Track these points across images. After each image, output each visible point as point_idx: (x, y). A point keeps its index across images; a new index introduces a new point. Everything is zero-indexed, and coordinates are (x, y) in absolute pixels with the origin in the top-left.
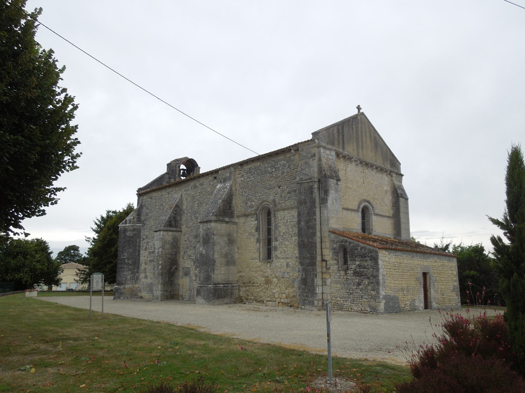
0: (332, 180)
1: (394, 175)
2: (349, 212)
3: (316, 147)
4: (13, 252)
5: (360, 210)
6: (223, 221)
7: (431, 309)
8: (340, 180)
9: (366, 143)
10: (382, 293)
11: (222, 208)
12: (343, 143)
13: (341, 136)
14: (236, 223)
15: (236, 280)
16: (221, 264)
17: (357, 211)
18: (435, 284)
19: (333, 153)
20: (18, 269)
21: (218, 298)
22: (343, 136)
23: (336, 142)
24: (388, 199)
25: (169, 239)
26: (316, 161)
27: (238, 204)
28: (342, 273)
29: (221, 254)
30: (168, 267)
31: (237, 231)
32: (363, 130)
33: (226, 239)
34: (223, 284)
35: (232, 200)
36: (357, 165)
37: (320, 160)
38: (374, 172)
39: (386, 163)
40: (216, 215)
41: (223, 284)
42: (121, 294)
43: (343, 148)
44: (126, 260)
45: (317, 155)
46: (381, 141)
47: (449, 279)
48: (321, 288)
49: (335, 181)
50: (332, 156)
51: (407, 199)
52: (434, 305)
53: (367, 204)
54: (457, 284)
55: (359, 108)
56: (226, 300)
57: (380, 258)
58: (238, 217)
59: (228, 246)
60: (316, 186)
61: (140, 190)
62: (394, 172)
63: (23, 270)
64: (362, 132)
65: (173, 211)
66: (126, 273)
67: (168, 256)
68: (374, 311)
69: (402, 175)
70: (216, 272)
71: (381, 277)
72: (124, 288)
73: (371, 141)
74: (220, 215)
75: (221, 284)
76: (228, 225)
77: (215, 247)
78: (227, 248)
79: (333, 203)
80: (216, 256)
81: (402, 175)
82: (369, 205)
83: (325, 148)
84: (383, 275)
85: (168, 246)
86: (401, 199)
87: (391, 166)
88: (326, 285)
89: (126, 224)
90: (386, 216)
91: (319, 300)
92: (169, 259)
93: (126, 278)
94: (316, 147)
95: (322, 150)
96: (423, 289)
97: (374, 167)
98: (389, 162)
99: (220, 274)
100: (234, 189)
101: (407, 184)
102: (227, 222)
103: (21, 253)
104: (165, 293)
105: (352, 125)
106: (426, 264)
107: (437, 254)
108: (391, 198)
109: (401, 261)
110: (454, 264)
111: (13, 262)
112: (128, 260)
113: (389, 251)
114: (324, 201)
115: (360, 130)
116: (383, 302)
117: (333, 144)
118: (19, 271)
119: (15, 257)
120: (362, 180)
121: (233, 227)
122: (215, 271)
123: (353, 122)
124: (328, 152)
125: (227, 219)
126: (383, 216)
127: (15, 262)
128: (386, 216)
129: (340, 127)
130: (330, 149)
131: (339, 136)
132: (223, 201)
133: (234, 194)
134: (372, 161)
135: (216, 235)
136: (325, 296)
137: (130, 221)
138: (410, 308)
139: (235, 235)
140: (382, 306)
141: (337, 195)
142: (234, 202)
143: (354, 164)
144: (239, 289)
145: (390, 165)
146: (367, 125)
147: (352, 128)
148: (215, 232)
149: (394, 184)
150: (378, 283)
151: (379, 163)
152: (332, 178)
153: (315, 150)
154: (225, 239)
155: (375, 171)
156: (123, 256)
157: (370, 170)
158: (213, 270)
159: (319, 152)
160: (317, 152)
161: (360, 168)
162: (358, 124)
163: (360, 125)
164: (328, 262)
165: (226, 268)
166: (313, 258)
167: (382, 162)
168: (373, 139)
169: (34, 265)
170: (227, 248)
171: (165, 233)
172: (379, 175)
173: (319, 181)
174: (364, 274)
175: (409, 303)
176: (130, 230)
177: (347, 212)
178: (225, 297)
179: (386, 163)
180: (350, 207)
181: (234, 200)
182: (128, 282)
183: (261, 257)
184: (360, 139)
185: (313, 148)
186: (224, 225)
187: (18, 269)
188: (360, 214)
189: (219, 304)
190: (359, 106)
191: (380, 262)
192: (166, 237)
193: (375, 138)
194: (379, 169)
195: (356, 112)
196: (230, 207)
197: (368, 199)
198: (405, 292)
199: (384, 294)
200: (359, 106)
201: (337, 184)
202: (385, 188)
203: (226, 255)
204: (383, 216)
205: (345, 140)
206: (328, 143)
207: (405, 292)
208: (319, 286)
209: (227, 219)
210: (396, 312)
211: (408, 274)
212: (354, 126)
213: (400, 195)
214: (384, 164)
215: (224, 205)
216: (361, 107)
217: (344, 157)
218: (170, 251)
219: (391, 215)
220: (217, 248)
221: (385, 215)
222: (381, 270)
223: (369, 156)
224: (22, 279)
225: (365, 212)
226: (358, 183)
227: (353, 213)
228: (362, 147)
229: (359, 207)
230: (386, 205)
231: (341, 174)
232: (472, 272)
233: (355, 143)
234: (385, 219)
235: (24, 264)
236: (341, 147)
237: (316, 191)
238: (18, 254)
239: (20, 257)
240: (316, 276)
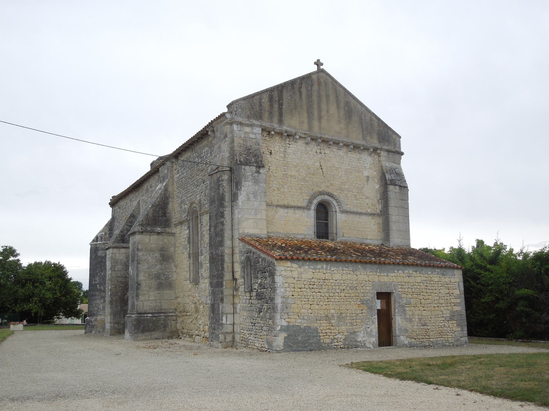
0: (247, 168)
1: (383, 153)
2: (291, 211)
3: (227, 123)
4: (22, 280)
5: (313, 207)
6: (152, 232)
7: (396, 346)
8: (263, 167)
9: (328, 112)
10: (281, 322)
11: (150, 215)
12: (281, 115)
13: (276, 106)
14: (173, 234)
15: (173, 307)
16: (150, 288)
17: (308, 208)
18: (407, 309)
19: (258, 130)
20: (27, 299)
21: (143, 331)
22: (281, 105)
23: (266, 115)
24: (373, 189)
25: (121, 258)
26: (227, 143)
27: (176, 210)
28: (248, 294)
29: (149, 275)
30: (119, 294)
31: (175, 244)
32: (323, 94)
33: (157, 255)
34: (152, 313)
35: (167, 204)
36: (307, 144)
37: (233, 142)
38: (342, 152)
39: (368, 138)
40: (142, 225)
41: (152, 313)
42: (93, 327)
43: (281, 122)
44: (98, 286)
45: (229, 136)
46: (359, 106)
47: (441, 301)
48: (230, 317)
49: (254, 169)
50: (256, 134)
51: (404, 188)
52: (403, 339)
53: (326, 197)
54: (460, 308)
55: (318, 63)
56: (156, 334)
57: (278, 273)
58: (176, 225)
59: (161, 264)
60: (226, 177)
61: (110, 204)
62: (381, 149)
63: (32, 300)
64: (319, 96)
65: (127, 222)
66: (98, 301)
67: (120, 279)
68: (268, 350)
69: (402, 154)
70: (141, 298)
71: (278, 301)
72: (96, 320)
73: (338, 107)
74: (149, 225)
75: (149, 313)
76: (161, 237)
77: (140, 266)
78: (159, 267)
79: (248, 199)
80: (141, 277)
81: (402, 154)
82: (331, 199)
83: (241, 124)
84: (283, 297)
85: (120, 267)
86: (391, 188)
87: (380, 142)
88: (236, 313)
89: (97, 241)
90: (366, 214)
91: (227, 333)
92: (122, 282)
93: (98, 308)
94: (227, 123)
95: (235, 127)
96: (376, 316)
97: (341, 144)
98: (375, 136)
99: (146, 300)
100: (170, 189)
101: (408, 166)
102: (158, 233)
103: (30, 280)
104: (116, 325)
105: (300, 88)
106: (386, 279)
107: (442, 267)
108: (377, 186)
109: (328, 276)
110: (456, 279)
111: (21, 291)
112: (100, 285)
113: (301, 263)
114: (234, 198)
115: (315, 94)
116: (283, 335)
117: (260, 117)
118: (29, 301)
119: (23, 286)
120: (318, 164)
121: (166, 239)
122: (140, 297)
123: (301, 84)
124: (247, 129)
125: (159, 229)
126: (361, 214)
127: (23, 291)
128: (366, 214)
129: (276, 93)
130: (252, 126)
131: (271, 106)
132: (153, 206)
133: (171, 195)
134: (342, 138)
135: (142, 250)
136: (237, 329)
137: (101, 238)
138: (344, 344)
139: (172, 249)
140: (280, 341)
141: (257, 188)
142: (170, 206)
143: (301, 143)
144: (176, 320)
145: (384, 140)
146: (330, 86)
147: (300, 93)
148: (140, 247)
149: (382, 167)
150: (273, 309)
151: (356, 138)
152: (247, 163)
153: (227, 129)
154: (156, 255)
155: (345, 149)
156: (95, 281)
157: (334, 149)
158: (137, 296)
159: (232, 131)
160: (229, 130)
161: (313, 148)
162: (312, 85)
163: (315, 87)
164: (238, 281)
165: (157, 292)
166: (221, 276)
167: (360, 137)
168: (342, 105)
169: (44, 295)
170: (159, 267)
171: (115, 250)
172: (354, 156)
173: (231, 170)
174: (263, 297)
175: (343, 337)
176: (102, 249)
177: (286, 210)
178: (154, 330)
179: (368, 138)
180: (292, 204)
181: (171, 204)
182: (101, 313)
183: (191, 277)
184: (315, 106)
185: (224, 125)
186: (155, 237)
187: (27, 299)
188: (312, 213)
189: (524, 346)
190: (318, 60)
191: (279, 279)
192: (118, 255)
193: (347, 104)
194: (352, 147)
195: (315, 68)
196: (165, 214)
197: (329, 190)
198: (333, 321)
199: (284, 323)
200: (318, 60)
201: (258, 172)
202: (366, 173)
203: (158, 276)
204: (361, 214)
205: (284, 111)
206: (249, 117)
207: (333, 321)
208: (227, 314)
209: (159, 229)
210: (311, 350)
211: (343, 295)
212: (304, 90)
213: (389, 182)
214: (364, 138)
215: (154, 211)
216: (321, 61)
217: (280, 134)
218: (123, 273)
219: (378, 211)
220: (144, 267)
221: (364, 211)
222: (280, 291)
223: (333, 127)
224: (31, 310)
225: (323, 211)
226: (309, 168)
227: (299, 213)
228: (320, 118)
229: (310, 202)
230: (367, 198)
231: (267, 158)
232: (529, 292)
233: (305, 115)
234: (364, 218)
235: (33, 293)
236: (276, 119)
237: (225, 184)
238: (26, 280)
239: (29, 285)
240: (222, 300)
